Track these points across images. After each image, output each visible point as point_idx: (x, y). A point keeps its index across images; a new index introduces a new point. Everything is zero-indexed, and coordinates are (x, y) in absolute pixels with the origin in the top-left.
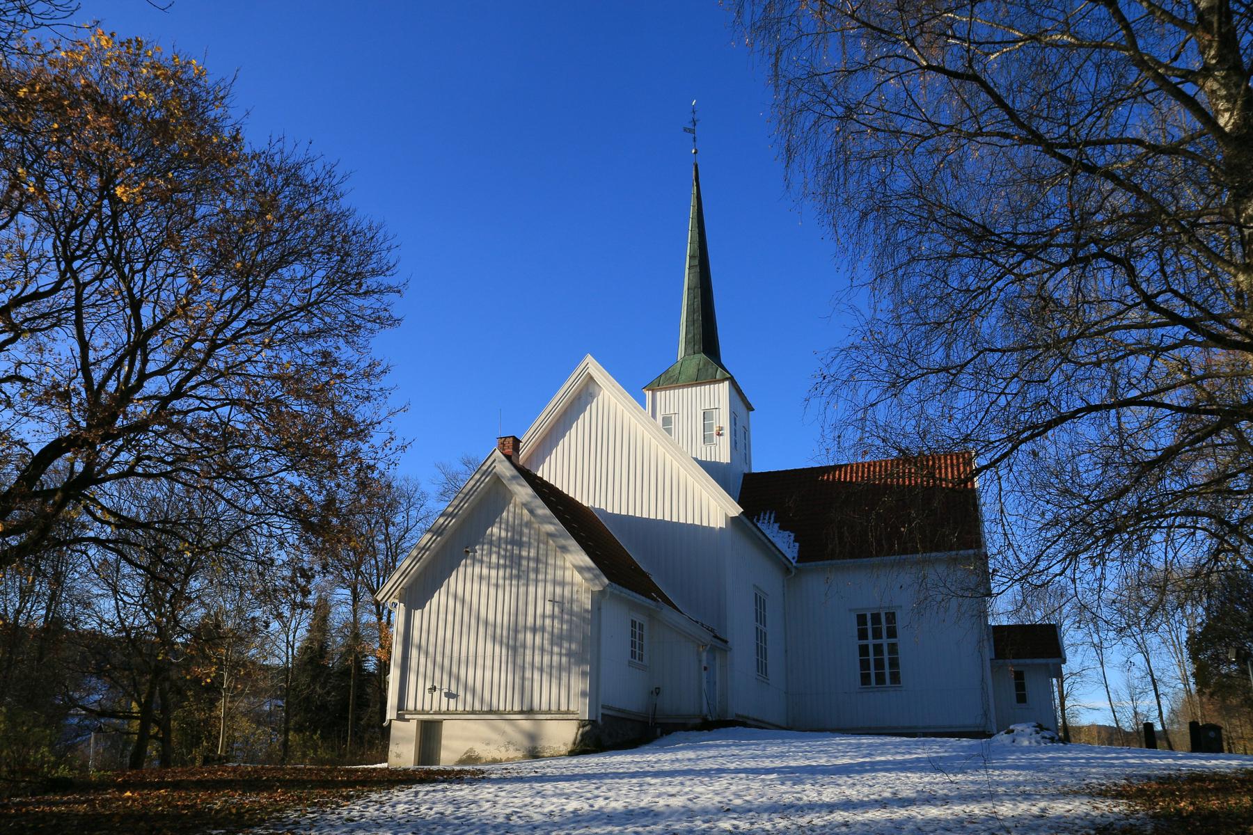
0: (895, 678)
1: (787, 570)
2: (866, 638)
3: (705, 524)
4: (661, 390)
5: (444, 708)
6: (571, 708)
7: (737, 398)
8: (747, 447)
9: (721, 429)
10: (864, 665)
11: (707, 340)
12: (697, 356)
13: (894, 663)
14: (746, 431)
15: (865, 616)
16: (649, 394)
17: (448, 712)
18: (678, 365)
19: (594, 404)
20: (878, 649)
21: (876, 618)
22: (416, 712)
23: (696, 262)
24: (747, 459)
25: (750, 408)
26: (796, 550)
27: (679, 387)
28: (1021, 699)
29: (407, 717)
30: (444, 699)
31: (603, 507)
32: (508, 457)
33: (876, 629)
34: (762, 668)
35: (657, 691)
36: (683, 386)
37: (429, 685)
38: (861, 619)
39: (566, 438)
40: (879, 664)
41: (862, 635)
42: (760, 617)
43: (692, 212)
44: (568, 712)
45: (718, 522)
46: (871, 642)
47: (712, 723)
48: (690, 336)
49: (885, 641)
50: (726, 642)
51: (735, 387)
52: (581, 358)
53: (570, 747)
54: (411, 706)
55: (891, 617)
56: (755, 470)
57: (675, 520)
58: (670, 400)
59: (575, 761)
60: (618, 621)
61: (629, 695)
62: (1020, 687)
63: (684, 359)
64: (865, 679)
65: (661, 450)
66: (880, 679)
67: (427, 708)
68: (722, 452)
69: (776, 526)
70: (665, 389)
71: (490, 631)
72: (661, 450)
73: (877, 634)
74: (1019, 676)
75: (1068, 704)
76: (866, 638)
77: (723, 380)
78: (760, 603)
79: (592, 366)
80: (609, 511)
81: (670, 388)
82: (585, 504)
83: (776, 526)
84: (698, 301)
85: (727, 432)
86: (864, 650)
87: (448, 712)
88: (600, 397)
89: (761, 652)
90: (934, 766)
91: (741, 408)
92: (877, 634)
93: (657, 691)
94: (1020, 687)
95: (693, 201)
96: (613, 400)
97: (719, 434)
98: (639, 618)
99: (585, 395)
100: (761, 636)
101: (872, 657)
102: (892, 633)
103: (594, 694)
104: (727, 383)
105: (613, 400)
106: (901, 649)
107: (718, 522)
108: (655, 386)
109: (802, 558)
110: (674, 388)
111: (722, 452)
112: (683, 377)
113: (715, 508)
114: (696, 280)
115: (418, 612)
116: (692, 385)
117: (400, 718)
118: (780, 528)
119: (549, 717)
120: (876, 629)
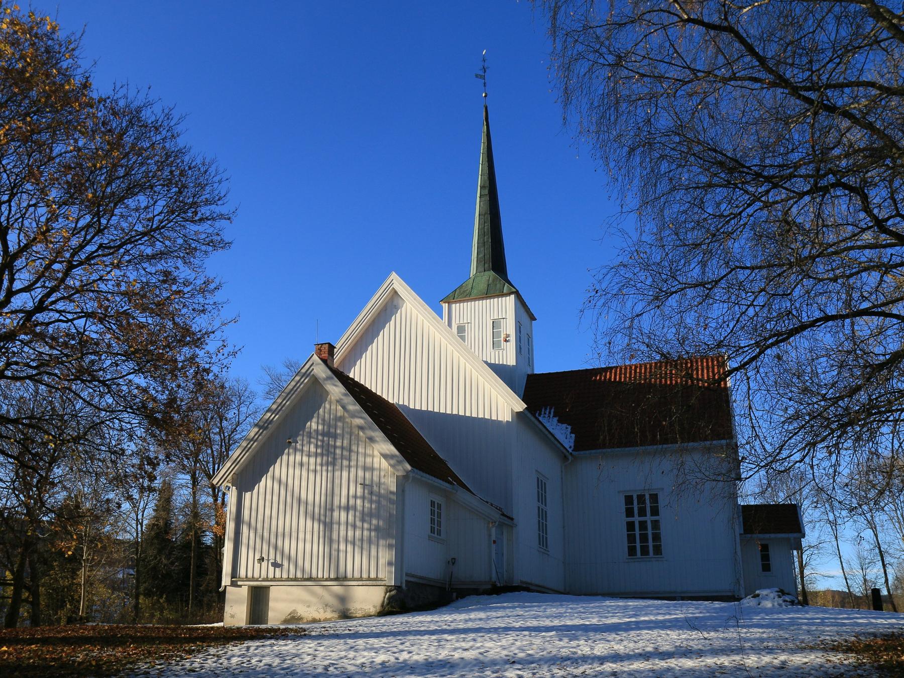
0: (658, 550)
1: (564, 456)
2: (640, 522)
3: (494, 418)
4: (456, 302)
5: (271, 576)
6: (380, 576)
7: (522, 310)
8: (530, 351)
9: (508, 336)
10: (631, 539)
11: (496, 259)
12: (487, 273)
13: (657, 537)
14: (529, 338)
15: (631, 497)
16: (445, 306)
17: (274, 579)
18: (471, 280)
19: (398, 315)
20: (643, 525)
21: (641, 498)
22: (247, 579)
23: (486, 192)
24: (530, 362)
25: (533, 318)
26: (572, 440)
27: (471, 300)
28: (766, 568)
29: (239, 583)
30: (271, 569)
31: (406, 403)
32: (325, 361)
33: (641, 508)
34: (543, 541)
35: (453, 561)
36: (475, 299)
37: (257, 557)
38: (629, 500)
39: (374, 344)
40: (644, 538)
41: (629, 512)
42: (542, 498)
43: (483, 147)
44: (376, 579)
45: (505, 416)
46: (637, 519)
47: (501, 588)
48: (481, 255)
49: (649, 518)
50: (512, 519)
51: (521, 301)
52: (388, 274)
53: (378, 609)
54: (242, 573)
55: (654, 498)
56: (538, 371)
57: (468, 414)
58: (464, 311)
59: (382, 620)
60: (420, 501)
61: (429, 565)
62: (765, 558)
63: (475, 276)
64: (632, 551)
65: (462, 361)
66: (645, 551)
67: (256, 575)
68: (509, 356)
69: (556, 419)
70: (460, 302)
71: (310, 508)
72: (462, 361)
73: (642, 512)
74: (765, 548)
75: (806, 572)
76: (640, 522)
77: (509, 294)
78: (541, 485)
79: (394, 276)
80: (412, 407)
81: (464, 301)
82: (391, 401)
83: (556, 419)
84: (488, 226)
85: (513, 338)
86: (630, 526)
87: (274, 579)
88: (403, 309)
89: (542, 528)
90: (690, 624)
91: (525, 318)
92: (642, 512)
93: (453, 561)
94: (765, 558)
95: (484, 139)
96: (415, 311)
97: (506, 341)
98: (438, 499)
99: (391, 306)
100: (542, 515)
101: (637, 532)
102: (655, 511)
103: (399, 563)
104: (513, 296)
105: (415, 311)
106: (662, 525)
107: (505, 416)
108: (451, 299)
109: (578, 446)
110: (467, 301)
111: (509, 356)
112: (475, 291)
113: (502, 404)
114: (486, 208)
115: (248, 495)
116: (483, 299)
117: (234, 584)
118: (559, 421)
119: (360, 583)
120: (641, 508)
